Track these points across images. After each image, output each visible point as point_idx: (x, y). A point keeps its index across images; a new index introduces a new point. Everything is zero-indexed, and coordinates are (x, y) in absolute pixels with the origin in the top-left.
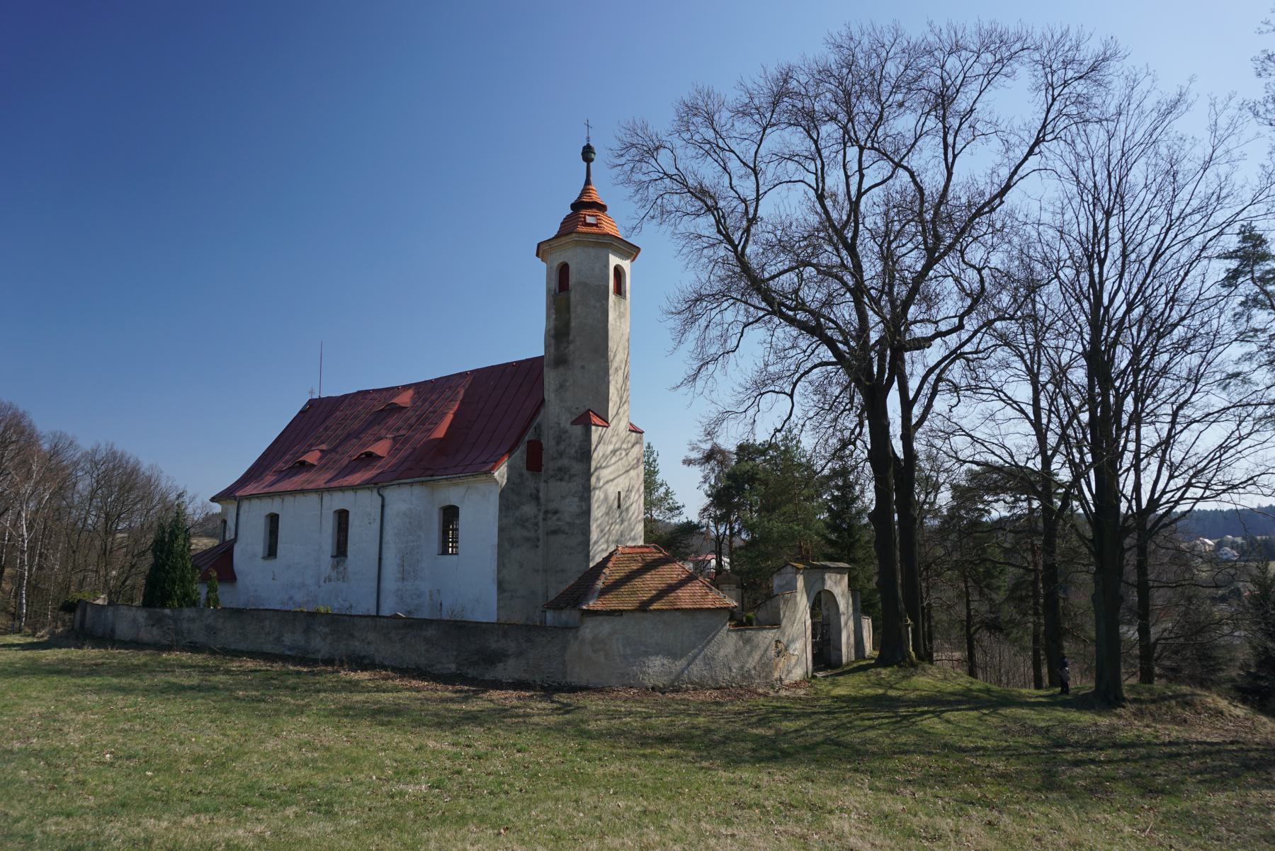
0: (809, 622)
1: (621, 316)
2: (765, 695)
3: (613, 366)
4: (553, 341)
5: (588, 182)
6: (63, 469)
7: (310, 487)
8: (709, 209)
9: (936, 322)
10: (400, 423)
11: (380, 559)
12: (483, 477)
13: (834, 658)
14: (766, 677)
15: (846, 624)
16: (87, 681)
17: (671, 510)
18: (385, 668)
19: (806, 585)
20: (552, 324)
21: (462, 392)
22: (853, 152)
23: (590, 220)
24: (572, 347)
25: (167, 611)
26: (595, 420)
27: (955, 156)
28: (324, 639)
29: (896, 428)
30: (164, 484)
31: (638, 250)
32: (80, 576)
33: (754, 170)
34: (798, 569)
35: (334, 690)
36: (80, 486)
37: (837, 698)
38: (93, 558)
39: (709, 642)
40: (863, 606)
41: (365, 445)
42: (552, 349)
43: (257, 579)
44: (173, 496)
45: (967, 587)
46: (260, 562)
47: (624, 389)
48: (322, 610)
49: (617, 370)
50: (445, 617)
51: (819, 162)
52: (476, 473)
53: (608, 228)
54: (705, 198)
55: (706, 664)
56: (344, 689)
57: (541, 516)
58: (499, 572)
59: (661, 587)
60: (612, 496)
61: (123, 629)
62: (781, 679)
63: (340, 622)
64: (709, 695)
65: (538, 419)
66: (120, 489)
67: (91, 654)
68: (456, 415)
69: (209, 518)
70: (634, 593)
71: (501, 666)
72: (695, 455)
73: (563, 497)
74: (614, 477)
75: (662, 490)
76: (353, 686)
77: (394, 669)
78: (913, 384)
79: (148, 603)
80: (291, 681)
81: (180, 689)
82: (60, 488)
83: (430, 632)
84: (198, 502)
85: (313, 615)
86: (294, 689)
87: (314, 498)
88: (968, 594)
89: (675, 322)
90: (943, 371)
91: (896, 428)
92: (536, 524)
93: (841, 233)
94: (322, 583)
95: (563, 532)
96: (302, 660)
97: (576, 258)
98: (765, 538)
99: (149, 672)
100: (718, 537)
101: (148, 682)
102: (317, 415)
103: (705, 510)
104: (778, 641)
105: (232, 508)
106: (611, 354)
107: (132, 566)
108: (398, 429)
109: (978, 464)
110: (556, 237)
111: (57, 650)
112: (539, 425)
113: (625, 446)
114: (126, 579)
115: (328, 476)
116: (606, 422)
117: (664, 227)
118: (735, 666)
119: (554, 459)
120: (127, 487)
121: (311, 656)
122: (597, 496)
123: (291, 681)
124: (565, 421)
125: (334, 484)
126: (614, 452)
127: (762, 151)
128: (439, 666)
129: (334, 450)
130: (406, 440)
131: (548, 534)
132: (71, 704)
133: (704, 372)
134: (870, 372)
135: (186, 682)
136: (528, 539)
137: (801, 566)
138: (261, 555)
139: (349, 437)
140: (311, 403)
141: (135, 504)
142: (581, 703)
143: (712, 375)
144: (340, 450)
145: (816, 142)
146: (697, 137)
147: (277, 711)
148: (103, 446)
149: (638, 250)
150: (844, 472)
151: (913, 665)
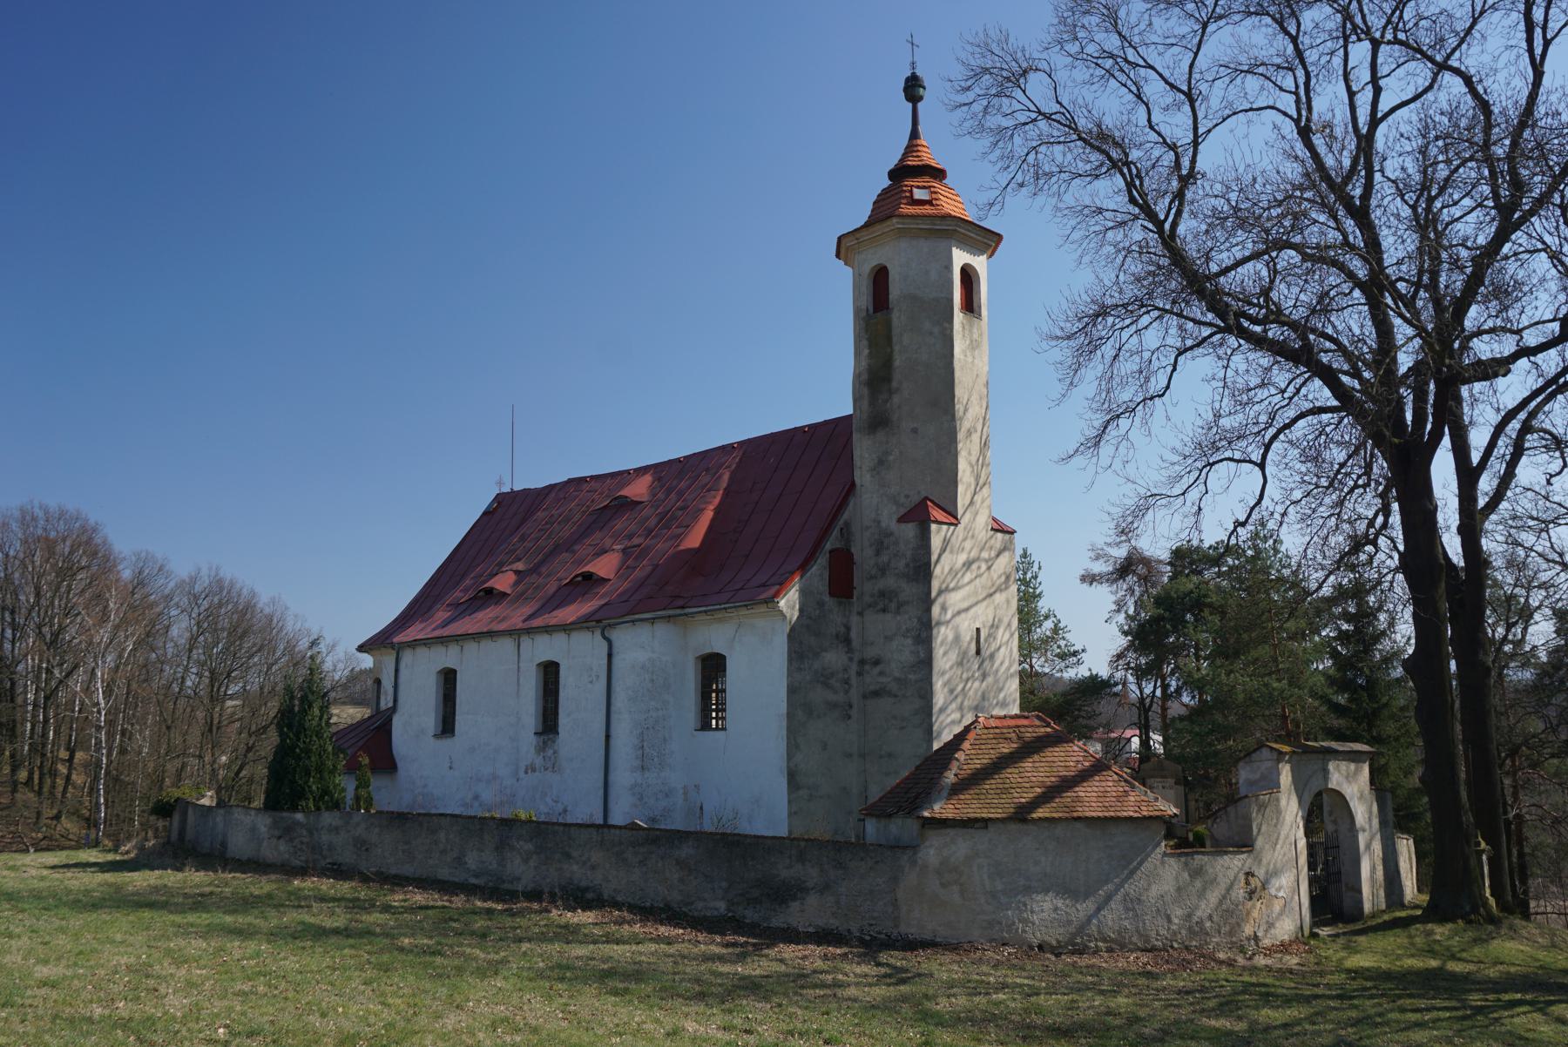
1: (974, 346)
2: (1230, 963)
3: (964, 427)
4: (866, 391)
5: (914, 134)
6: (152, 606)
7: (502, 626)
8: (1114, 165)
9: (1519, 332)
10: (633, 527)
11: (608, 737)
12: (763, 608)
14: (1231, 933)
15: (1368, 846)
16: (191, 918)
17: (1062, 657)
18: (617, 905)
21: (726, 477)
22: (1360, 51)
23: (919, 194)
24: (896, 399)
25: (299, 816)
26: (936, 513)
27: (1547, 43)
28: (526, 861)
31: (998, 238)
32: (178, 763)
33: (1189, 95)
34: (1280, 753)
35: (542, 938)
36: (174, 632)
39: (1132, 873)
40: (1396, 818)
41: (580, 562)
42: (865, 403)
43: (429, 769)
44: (303, 644)
47: (981, 463)
48: (523, 816)
49: (969, 433)
50: (708, 827)
51: (1300, 73)
52: (751, 602)
53: (949, 206)
54: (1107, 148)
55: (1127, 909)
56: (557, 937)
57: (854, 667)
58: (790, 757)
60: (967, 636)
61: (239, 843)
62: (1256, 938)
63: (549, 835)
65: (845, 516)
66: (230, 634)
67: (195, 878)
68: (718, 511)
69: (355, 677)
70: (1006, 791)
72: (1100, 567)
73: (888, 639)
74: (968, 607)
75: (1048, 624)
76: (570, 934)
77: (632, 908)
78: (1478, 439)
79: (272, 805)
80: (480, 923)
81: (320, 933)
83: (686, 851)
84: (340, 652)
86: (484, 936)
87: (507, 644)
89: (1062, 353)
92: (847, 682)
94: (522, 774)
95: (890, 694)
96: (494, 892)
98: (1223, 702)
100: (1142, 700)
101: (274, 922)
102: (510, 518)
103: (1119, 656)
104: (1249, 874)
105: (389, 660)
106: (959, 408)
107: (249, 749)
108: (630, 537)
110: (867, 225)
111: (147, 873)
112: (847, 524)
113: (985, 555)
115: (527, 610)
116: (953, 518)
117: (1041, 199)
118: (1177, 913)
120: (240, 631)
121: (506, 886)
122: (942, 635)
126: (968, 564)
128: (700, 905)
130: (644, 552)
131: (865, 697)
133: (1112, 432)
134: (1400, 423)
135: (329, 923)
136: (833, 706)
137: (1286, 749)
139: (556, 550)
140: (501, 499)
141: (252, 656)
144: (543, 569)
147: (460, 970)
148: (204, 572)
149: (998, 238)
150: (1358, 591)
151: (1492, 920)
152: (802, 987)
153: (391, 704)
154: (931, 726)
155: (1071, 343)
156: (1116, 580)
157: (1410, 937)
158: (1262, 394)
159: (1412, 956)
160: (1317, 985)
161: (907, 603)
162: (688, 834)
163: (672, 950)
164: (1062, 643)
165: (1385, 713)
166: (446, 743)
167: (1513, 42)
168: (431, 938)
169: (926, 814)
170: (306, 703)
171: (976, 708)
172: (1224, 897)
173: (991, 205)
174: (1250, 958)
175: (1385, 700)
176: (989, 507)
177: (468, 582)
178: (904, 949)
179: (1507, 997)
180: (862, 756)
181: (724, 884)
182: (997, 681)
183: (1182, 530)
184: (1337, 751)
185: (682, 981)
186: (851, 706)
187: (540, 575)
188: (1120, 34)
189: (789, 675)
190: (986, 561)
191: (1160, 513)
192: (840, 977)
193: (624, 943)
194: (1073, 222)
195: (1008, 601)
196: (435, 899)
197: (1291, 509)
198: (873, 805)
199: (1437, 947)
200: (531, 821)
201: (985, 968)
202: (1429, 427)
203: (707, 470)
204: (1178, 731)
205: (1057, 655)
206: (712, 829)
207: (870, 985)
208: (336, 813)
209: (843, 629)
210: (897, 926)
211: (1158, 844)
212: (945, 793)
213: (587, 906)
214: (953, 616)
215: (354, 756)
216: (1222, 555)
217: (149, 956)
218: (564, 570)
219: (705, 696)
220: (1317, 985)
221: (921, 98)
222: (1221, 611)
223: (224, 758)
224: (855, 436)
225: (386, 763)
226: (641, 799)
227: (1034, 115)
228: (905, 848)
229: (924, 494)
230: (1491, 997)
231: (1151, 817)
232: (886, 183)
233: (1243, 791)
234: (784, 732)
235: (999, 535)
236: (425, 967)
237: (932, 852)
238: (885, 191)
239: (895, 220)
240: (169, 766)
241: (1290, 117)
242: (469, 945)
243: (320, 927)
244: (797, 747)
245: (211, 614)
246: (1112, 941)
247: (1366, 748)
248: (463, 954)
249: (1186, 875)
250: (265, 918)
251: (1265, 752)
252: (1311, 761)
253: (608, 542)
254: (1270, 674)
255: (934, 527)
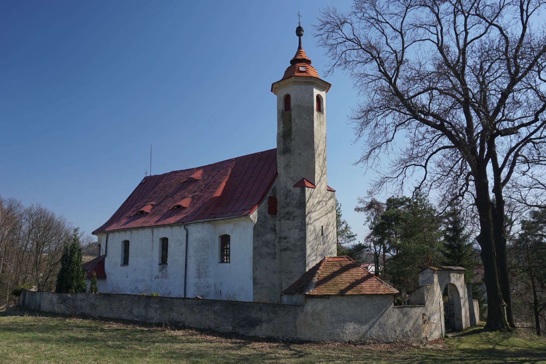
0: (442, 303)
1: (321, 124)
2: (418, 347)
3: (317, 153)
4: (282, 140)
5: (300, 48)
6: (15, 218)
7: (147, 225)
8: (374, 58)
9: (513, 121)
10: (195, 189)
11: (186, 265)
12: (244, 218)
13: (457, 325)
14: (418, 336)
15: (464, 305)
16: (26, 335)
17: (349, 237)
18: (191, 328)
19: (439, 281)
20: (281, 129)
21: (230, 171)
22: (460, 19)
23: (301, 69)
24: (293, 142)
25: (69, 295)
26: (307, 184)
27: (528, 17)
28: (156, 312)
29: (491, 183)
30: (67, 226)
31: (330, 85)
32: (24, 276)
33: (401, 33)
34: (434, 270)
35: (163, 341)
36: (24, 228)
37: (464, 350)
38: (30, 266)
39: (382, 314)
40: (473, 295)
41: (176, 201)
42: (282, 144)
43: (118, 278)
44: (72, 233)
45: (533, 283)
46: (119, 268)
47: (323, 166)
48: (155, 295)
49: (319, 155)
50: (224, 298)
51: (439, 28)
52: (240, 216)
53: (312, 73)
54: (372, 52)
55: (380, 328)
56: (168, 341)
57: (277, 240)
58: (254, 273)
59: (353, 281)
60: (318, 229)
61: (45, 306)
62: (426, 338)
63: (165, 301)
64: (382, 347)
65: (274, 185)
66: (44, 229)
67: (28, 319)
68: (227, 183)
69: (90, 245)
70: (336, 285)
71: (258, 328)
72: (361, 206)
73: (290, 229)
74: (318, 218)
75: (344, 226)
76: (174, 339)
77: (196, 329)
78: (500, 160)
79: (59, 291)
80: (138, 336)
81: (77, 340)
82: (13, 229)
83: (217, 307)
84: (85, 236)
85: (149, 297)
86: (140, 341)
87: (149, 231)
88: (534, 287)
89: (356, 124)
90: (519, 150)
91: (491, 183)
92: (274, 245)
93: (453, 68)
94: (153, 279)
95: (291, 250)
96: (144, 324)
97: (294, 91)
98: (406, 253)
99: (60, 330)
100: (376, 253)
101: (58, 336)
102: (149, 186)
103: (368, 237)
104: (424, 315)
105: (104, 238)
106: (316, 146)
107: (51, 271)
108: (194, 192)
109: (540, 207)
110: (282, 80)
111: (9, 317)
112: (275, 188)
113: (325, 199)
114: (47, 278)
115: (156, 219)
116: (314, 186)
117: (346, 70)
118: (398, 329)
119: (284, 207)
120: (48, 228)
121: (148, 321)
122: (310, 228)
123: (138, 336)
124: (290, 185)
125: (159, 223)
126: (319, 203)
127: (404, 24)
128: (222, 328)
129: (159, 204)
130: (199, 198)
131: (281, 251)
132: (15, 349)
133: (373, 154)
134: (474, 153)
135: (80, 336)
136: (269, 254)
137: (436, 269)
138: (119, 263)
139: (167, 197)
140: (147, 179)
141: (52, 237)
142: (308, 350)
143: (377, 156)
144: (162, 204)
145: (437, 15)
146: (366, 15)
147: (132, 355)
148: (35, 206)
149: (330, 85)
150: (455, 213)
151: (509, 330)
152: (264, 359)
153: (104, 254)
154: (305, 261)
155: (359, 121)
156: (367, 210)
157: (481, 337)
158: (424, 142)
159: (482, 344)
160: (451, 355)
161: (297, 216)
162: (218, 301)
163: (212, 345)
164: (349, 232)
165: (464, 256)
166: (126, 268)
167: (515, 16)
168: (120, 341)
169: (307, 293)
170: (72, 252)
171: (321, 255)
172: (415, 323)
173: (329, 72)
174: (425, 346)
175: (464, 252)
176: (326, 182)
177: (134, 209)
178: (299, 344)
179: (520, 359)
180: (280, 272)
181: (231, 320)
182: (328, 245)
183: (396, 190)
184: (453, 270)
185: (218, 358)
186: (276, 254)
187: (161, 206)
188: (376, 10)
189: (254, 242)
190: (325, 201)
191: (389, 184)
192: (277, 355)
193: (194, 343)
194: (357, 80)
195: (333, 216)
196: (121, 326)
197: (433, 184)
198: (286, 290)
199: (491, 340)
200: (158, 297)
201: (330, 351)
202: (486, 153)
203: (223, 168)
204: (391, 264)
205: (347, 237)
206: (226, 299)
207: (289, 358)
208: (83, 294)
209: (273, 226)
210: (296, 335)
211: (391, 304)
212: (314, 286)
213: (179, 329)
214: (313, 221)
215: (91, 272)
216: (405, 202)
217: (7, 350)
218: (170, 204)
219: (222, 250)
220: (451, 355)
221: (302, 35)
222: (405, 221)
223: (41, 275)
224: (277, 155)
225: (102, 275)
226: (198, 288)
227: (344, 40)
228: (299, 306)
229: (303, 177)
230: (514, 359)
231: (389, 294)
232: (290, 65)
233: (420, 285)
234: (252, 264)
235: (330, 192)
236: (118, 354)
237: (309, 307)
238: (289, 68)
239: (293, 78)
240: (20, 277)
241: (435, 43)
242: (135, 344)
243: (77, 338)
244: (257, 269)
245: (37, 221)
246: (375, 339)
247: (463, 268)
248: (133, 348)
249: (401, 315)
250: (55, 334)
251: (429, 270)
252: (445, 273)
253: (186, 194)
254: (423, 243)
255: (307, 189)
